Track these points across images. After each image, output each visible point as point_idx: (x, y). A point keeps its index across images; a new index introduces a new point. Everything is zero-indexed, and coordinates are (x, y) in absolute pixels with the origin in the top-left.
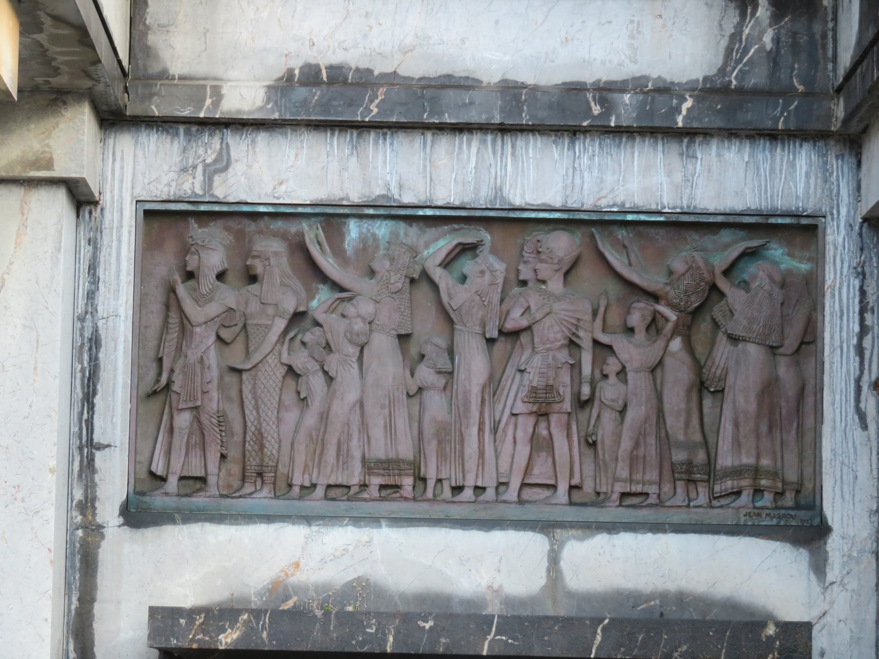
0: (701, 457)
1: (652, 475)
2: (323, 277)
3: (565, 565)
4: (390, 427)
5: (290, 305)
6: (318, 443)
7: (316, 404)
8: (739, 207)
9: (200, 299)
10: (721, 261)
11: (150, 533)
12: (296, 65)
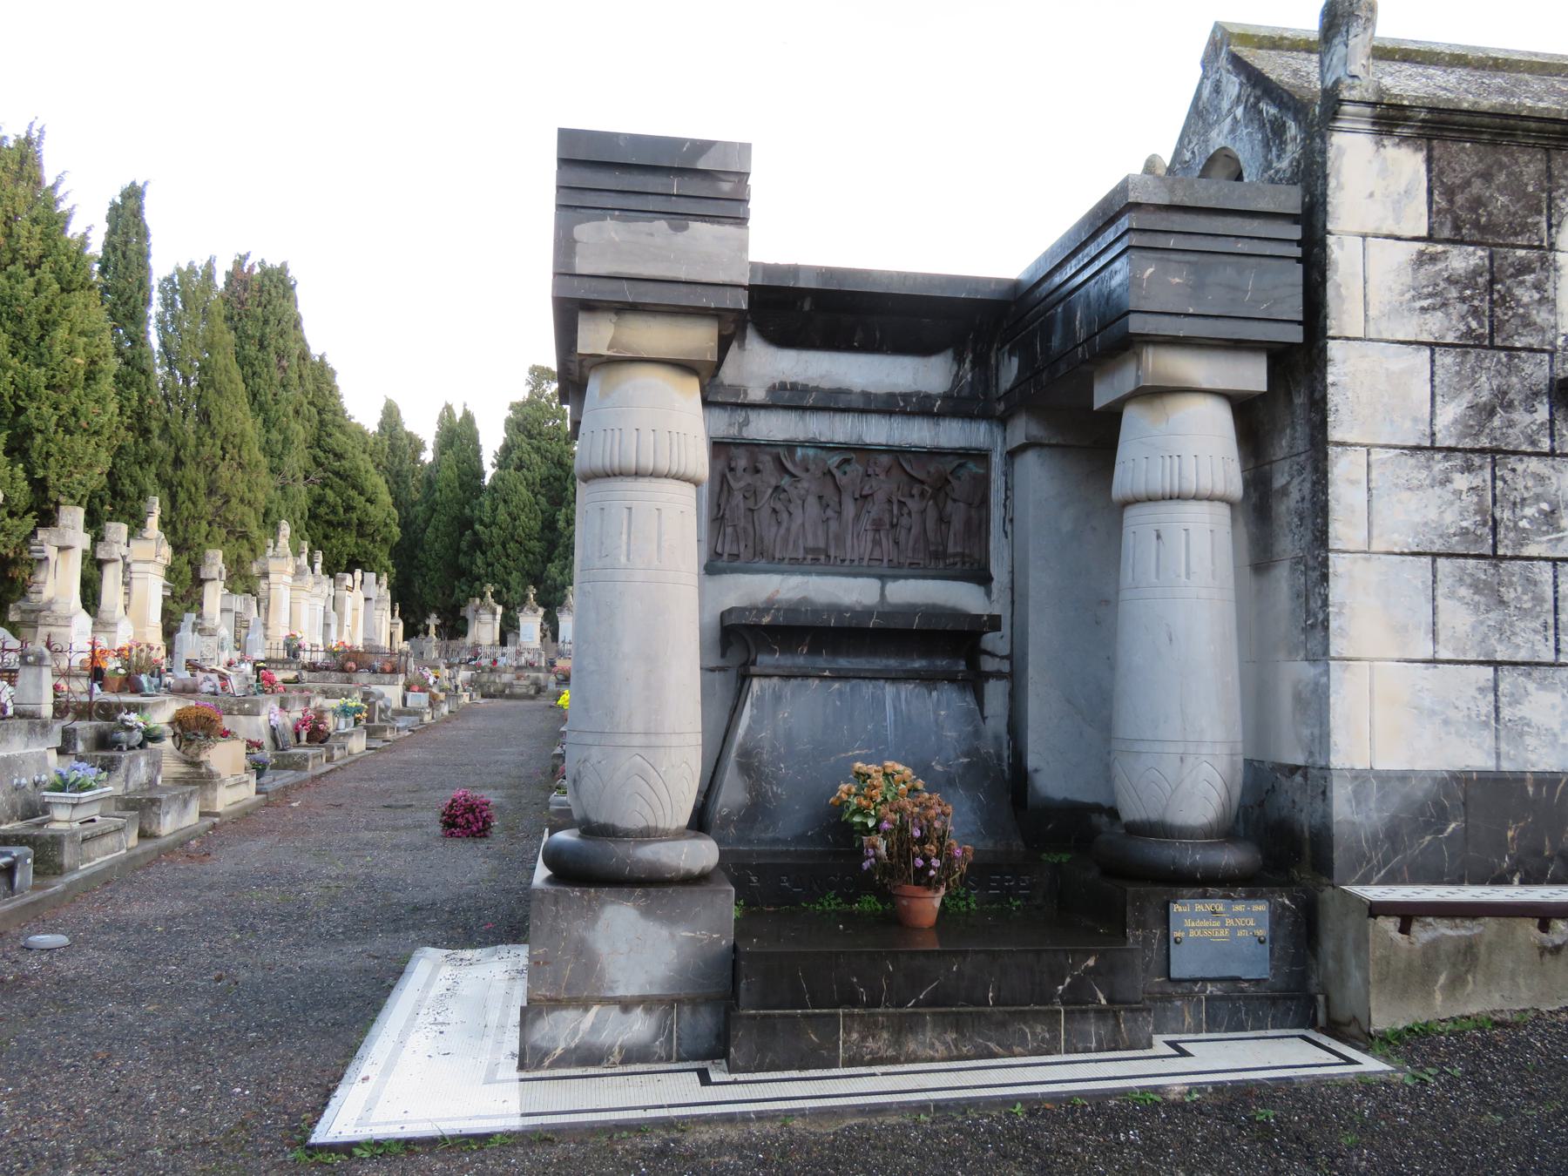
0: (941, 548)
1: (921, 555)
2: (786, 471)
3: (887, 592)
4: (815, 535)
5: (773, 482)
6: (786, 541)
7: (785, 525)
8: (957, 446)
9: (738, 480)
10: (949, 468)
11: (717, 578)
12: (777, 381)
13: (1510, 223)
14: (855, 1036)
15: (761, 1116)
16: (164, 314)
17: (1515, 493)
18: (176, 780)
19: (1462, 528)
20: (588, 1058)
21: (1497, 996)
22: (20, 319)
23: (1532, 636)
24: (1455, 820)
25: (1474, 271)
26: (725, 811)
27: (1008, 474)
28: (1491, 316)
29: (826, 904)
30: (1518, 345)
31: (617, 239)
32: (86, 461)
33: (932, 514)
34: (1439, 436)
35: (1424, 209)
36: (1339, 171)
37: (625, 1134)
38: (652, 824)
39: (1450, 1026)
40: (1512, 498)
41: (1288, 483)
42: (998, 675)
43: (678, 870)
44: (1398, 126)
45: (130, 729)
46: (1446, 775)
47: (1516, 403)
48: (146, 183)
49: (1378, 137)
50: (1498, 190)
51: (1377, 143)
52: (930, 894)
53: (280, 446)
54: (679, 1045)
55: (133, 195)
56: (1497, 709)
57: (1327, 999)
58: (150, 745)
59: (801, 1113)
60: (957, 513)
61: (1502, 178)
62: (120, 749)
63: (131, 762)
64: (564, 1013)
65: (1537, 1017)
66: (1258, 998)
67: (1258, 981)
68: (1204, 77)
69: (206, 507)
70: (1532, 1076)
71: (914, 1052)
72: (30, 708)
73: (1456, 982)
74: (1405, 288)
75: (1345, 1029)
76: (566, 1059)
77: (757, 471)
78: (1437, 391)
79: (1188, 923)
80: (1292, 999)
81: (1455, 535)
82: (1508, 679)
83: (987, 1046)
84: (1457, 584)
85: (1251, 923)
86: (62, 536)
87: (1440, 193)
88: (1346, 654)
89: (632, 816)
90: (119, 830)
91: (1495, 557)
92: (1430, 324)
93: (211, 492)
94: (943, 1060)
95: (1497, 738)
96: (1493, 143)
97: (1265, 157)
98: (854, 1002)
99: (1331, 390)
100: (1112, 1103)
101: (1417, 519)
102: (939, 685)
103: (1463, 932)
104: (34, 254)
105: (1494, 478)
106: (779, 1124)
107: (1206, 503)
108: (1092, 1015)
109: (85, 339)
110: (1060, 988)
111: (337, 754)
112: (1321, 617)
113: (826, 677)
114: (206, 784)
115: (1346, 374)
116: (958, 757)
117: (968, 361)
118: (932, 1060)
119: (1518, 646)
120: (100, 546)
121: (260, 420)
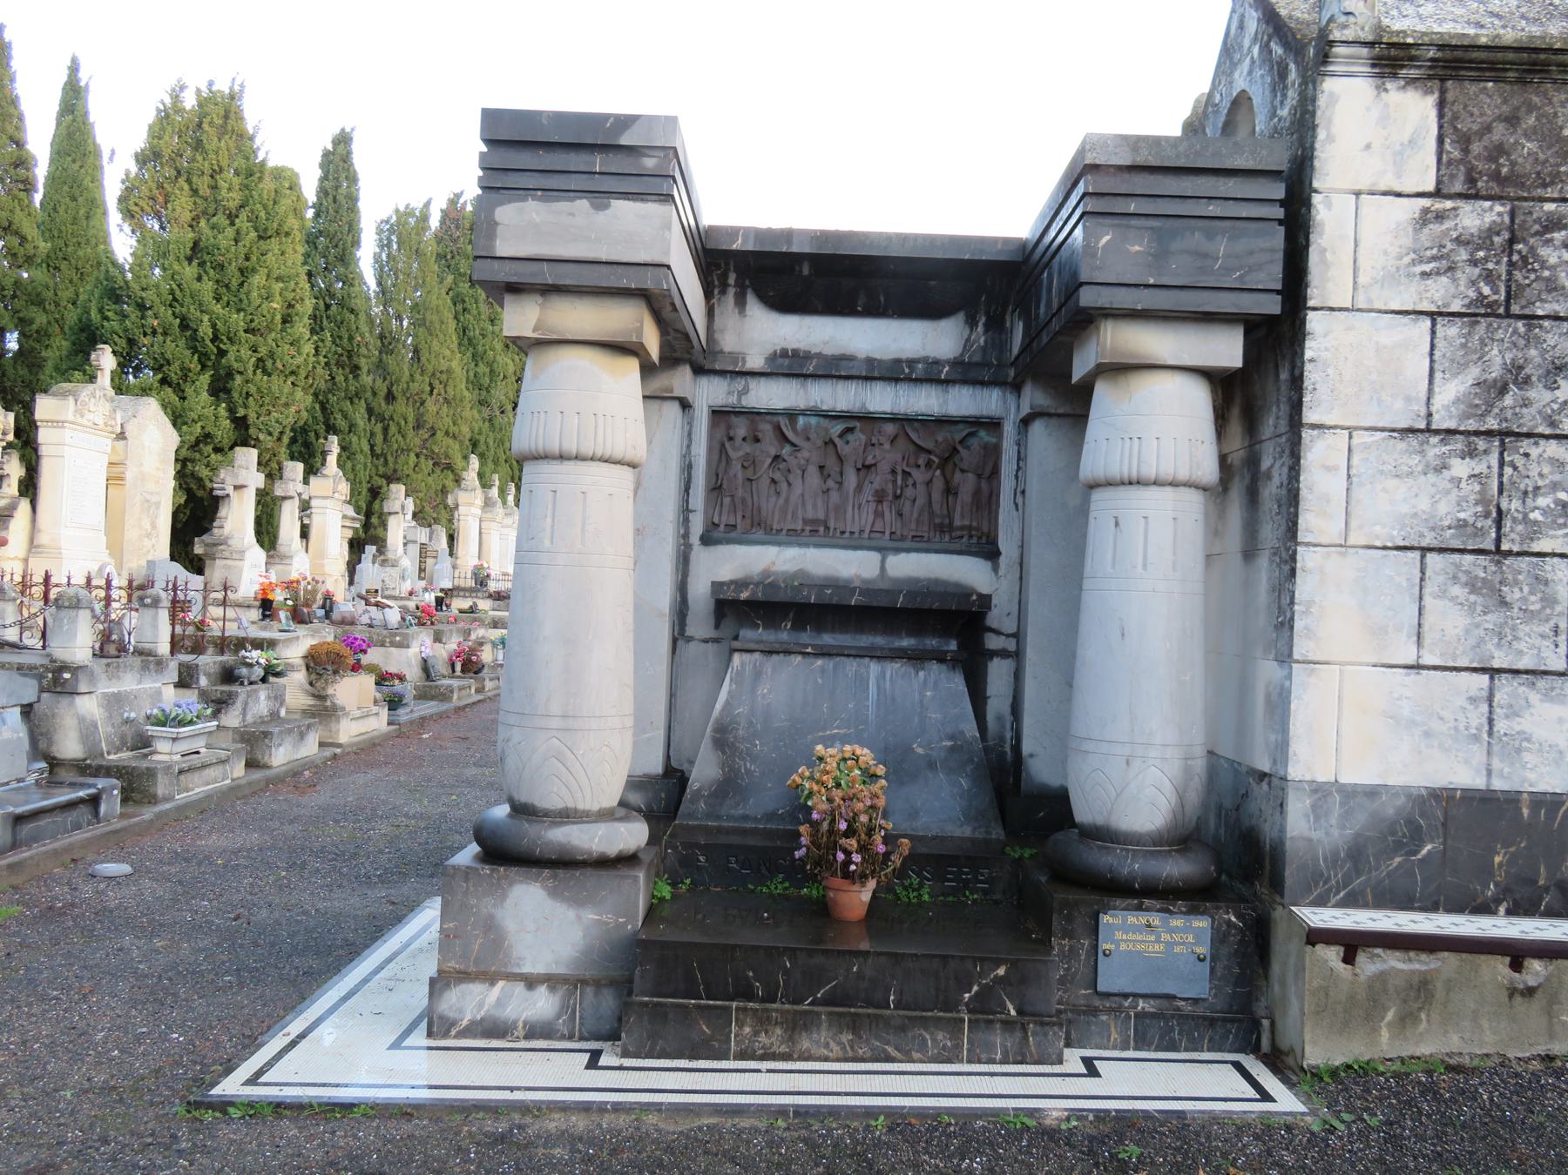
0: (947, 521)
1: (926, 528)
2: (786, 439)
4: (815, 506)
5: (773, 452)
6: (784, 512)
7: (784, 495)
9: (735, 449)
10: (959, 437)
11: (712, 548)
12: (778, 348)
13: (1538, 173)
14: (747, 1030)
15: (618, 1108)
16: (380, 253)
17: (1527, 481)
18: (304, 712)
19: (1459, 520)
20: (493, 1030)
21: (1455, 1038)
22: (222, 267)
23: (1538, 642)
24: (1432, 841)
25: (1490, 229)
26: (696, 786)
27: (1021, 444)
28: (1508, 280)
29: (773, 887)
30: (1540, 312)
31: (538, 220)
32: (283, 400)
33: (938, 485)
34: (1436, 417)
35: (1433, 161)
36: (1330, 121)
37: (480, 1115)
38: (571, 805)
39: (1396, 1066)
40: (1522, 487)
41: (1272, 466)
42: (1004, 654)
43: (590, 853)
44: (1402, 67)
45: (250, 665)
46: (1424, 792)
47: (1534, 379)
48: (353, 130)
49: (1379, 81)
50: (1526, 135)
51: (1377, 88)
52: (856, 887)
53: (487, 380)
54: (581, 1024)
55: (343, 140)
56: (1491, 721)
57: (1273, 1024)
58: (272, 679)
59: (657, 1108)
60: (966, 484)
61: (1532, 121)
62: (242, 684)
63: (248, 696)
64: (471, 986)
65: (1502, 1065)
66: (1193, 1018)
67: (1196, 1001)
68: (1233, 11)
69: (414, 440)
70: (1456, 1134)
71: (808, 1050)
72: (147, 646)
73: (1406, 1020)
74: (1404, 251)
75: (1284, 1058)
76: (473, 1030)
77: (757, 440)
78: (1436, 366)
79: (1119, 935)
80: (1232, 1021)
81: (1450, 528)
82: (1505, 687)
83: (885, 1051)
84: (1449, 582)
85: (1191, 939)
86: (236, 476)
87: (1453, 141)
88: (1311, 657)
89: (550, 797)
90: (222, 762)
91: (1499, 553)
92: (1433, 291)
93: (418, 426)
94: (838, 1060)
95: (1489, 753)
96: (1521, 81)
97: (1272, 103)
98: (749, 995)
99: (1308, 367)
100: (980, 1123)
101: (1405, 509)
102: (926, 664)
103: (1417, 966)
104: (232, 205)
105: (1502, 464)
106: (634, 1117)
107: (1169, 489)
108: (998, 1026)
109: (281, 285)
110: (967, 995)
111: (489, 685)
112: (1288, 615)
113: (809, 654)
114: (330, 716)
115: (1327, 349)
116: (941, 740)
117: (980, 324)
118: (826, 1059)
119: (1521, 653)
120: (278, 484)
121: (469, 354)
